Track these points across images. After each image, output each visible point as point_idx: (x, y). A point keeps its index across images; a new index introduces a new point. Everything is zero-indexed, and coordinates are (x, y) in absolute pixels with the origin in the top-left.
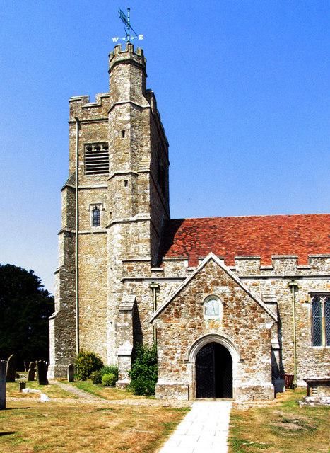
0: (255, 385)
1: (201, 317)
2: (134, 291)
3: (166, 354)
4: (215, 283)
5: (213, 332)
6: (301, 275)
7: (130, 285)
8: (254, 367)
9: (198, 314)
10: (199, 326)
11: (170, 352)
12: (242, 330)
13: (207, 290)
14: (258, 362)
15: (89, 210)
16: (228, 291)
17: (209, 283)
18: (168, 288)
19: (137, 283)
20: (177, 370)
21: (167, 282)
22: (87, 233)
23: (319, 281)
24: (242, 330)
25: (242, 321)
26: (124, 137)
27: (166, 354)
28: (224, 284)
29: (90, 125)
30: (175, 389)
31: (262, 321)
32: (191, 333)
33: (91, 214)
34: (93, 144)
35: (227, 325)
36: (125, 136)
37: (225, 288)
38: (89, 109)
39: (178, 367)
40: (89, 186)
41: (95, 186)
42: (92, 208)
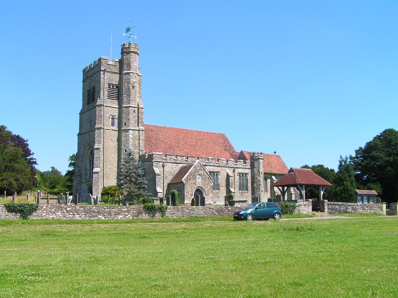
0: (210, 203)
1: (196, 180)
2: (157, 166)
3: (187, 192)
4: (199, 170)
5: (199, 185)
6: (207, 164)
7: (156, 164)
8: (209, 197)
9: (195, 179)
10: (195, 183)
11: (188, 192)
12: (206, 185)
13: (197, 172)
14: (210, 196)
15: (109, 118)
16: (203, 172)
17: (198, 169)
18: (168, 166)
19: (158, 163)
20: (190, 198)
21: (168, 164)
22: (109, 129)
23: (212, 167)
24: (206, 185)
25: (206, 182)
26: (133, 89)
27: (187, 192)
28: (201, 170)
29: (111, 74)
30: (49, 234)
31: (211, 183)
32: (193, 186)
33: (111, 119)
34: (112, 84)
35: (202, 184)
36: (134, 89)
37: (202, 171)
38: (110, 65)
39: (190, 197)
40: (110, 106)
41: (113, 106)
42: (111, 117)
